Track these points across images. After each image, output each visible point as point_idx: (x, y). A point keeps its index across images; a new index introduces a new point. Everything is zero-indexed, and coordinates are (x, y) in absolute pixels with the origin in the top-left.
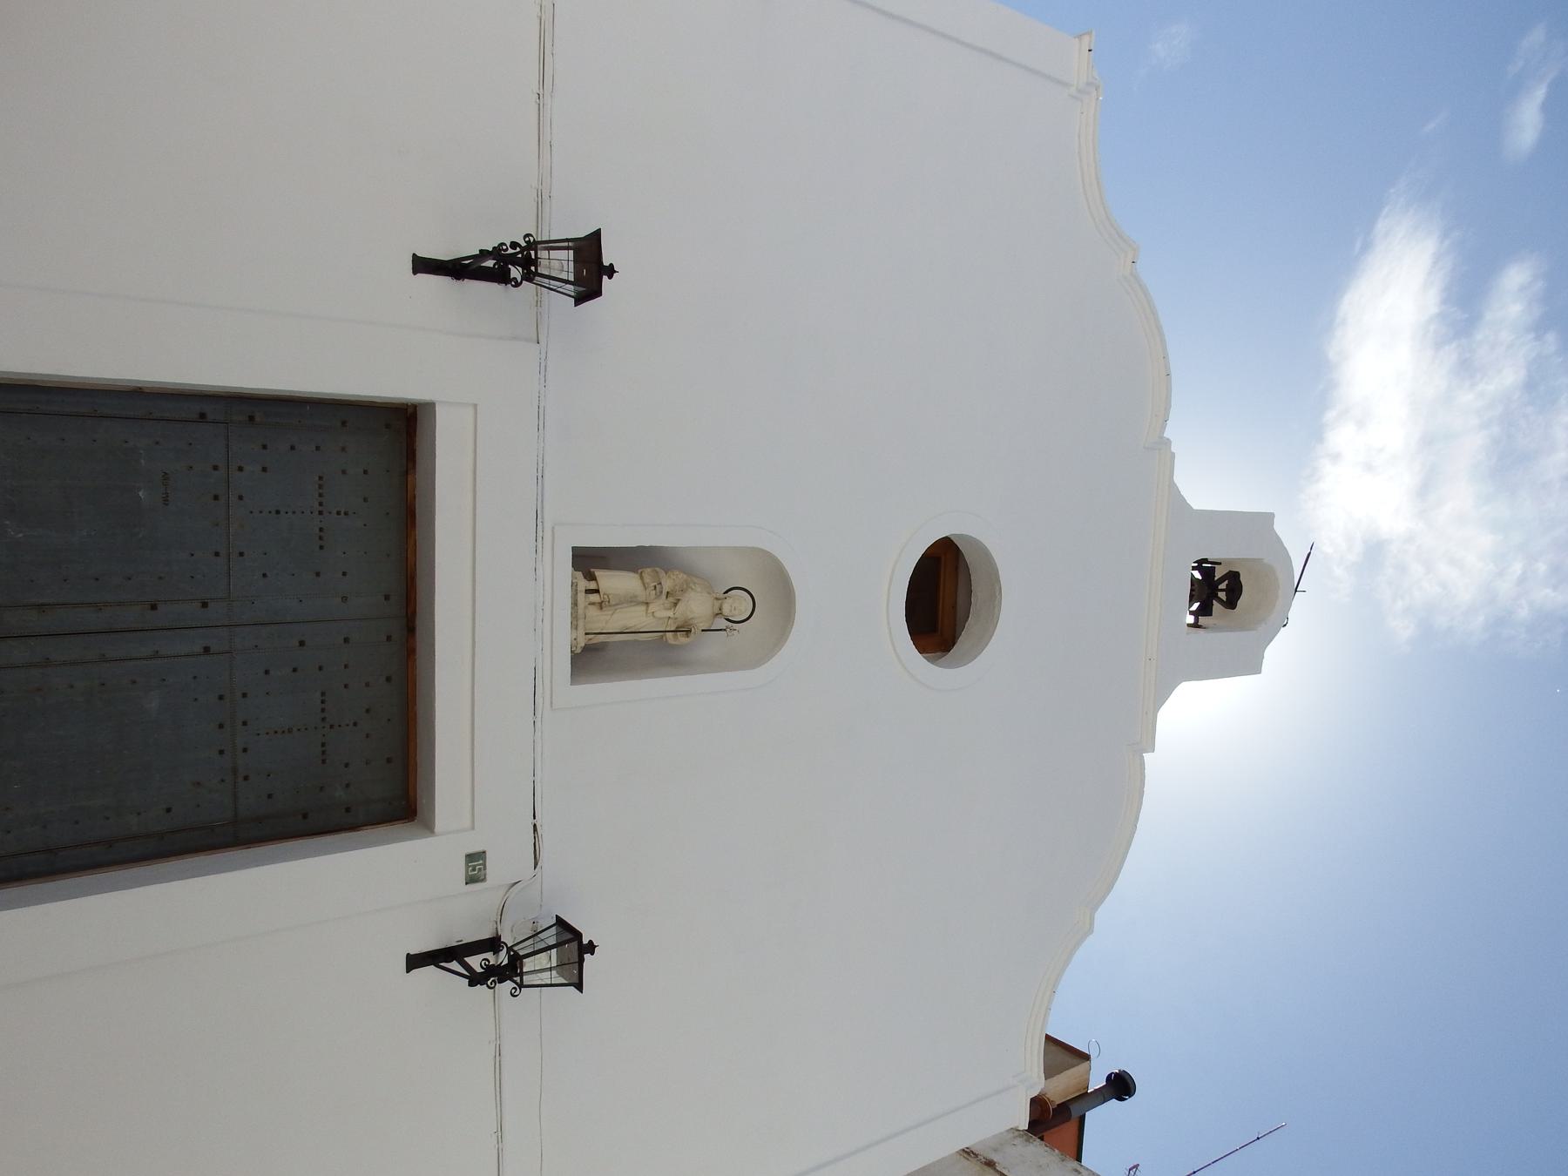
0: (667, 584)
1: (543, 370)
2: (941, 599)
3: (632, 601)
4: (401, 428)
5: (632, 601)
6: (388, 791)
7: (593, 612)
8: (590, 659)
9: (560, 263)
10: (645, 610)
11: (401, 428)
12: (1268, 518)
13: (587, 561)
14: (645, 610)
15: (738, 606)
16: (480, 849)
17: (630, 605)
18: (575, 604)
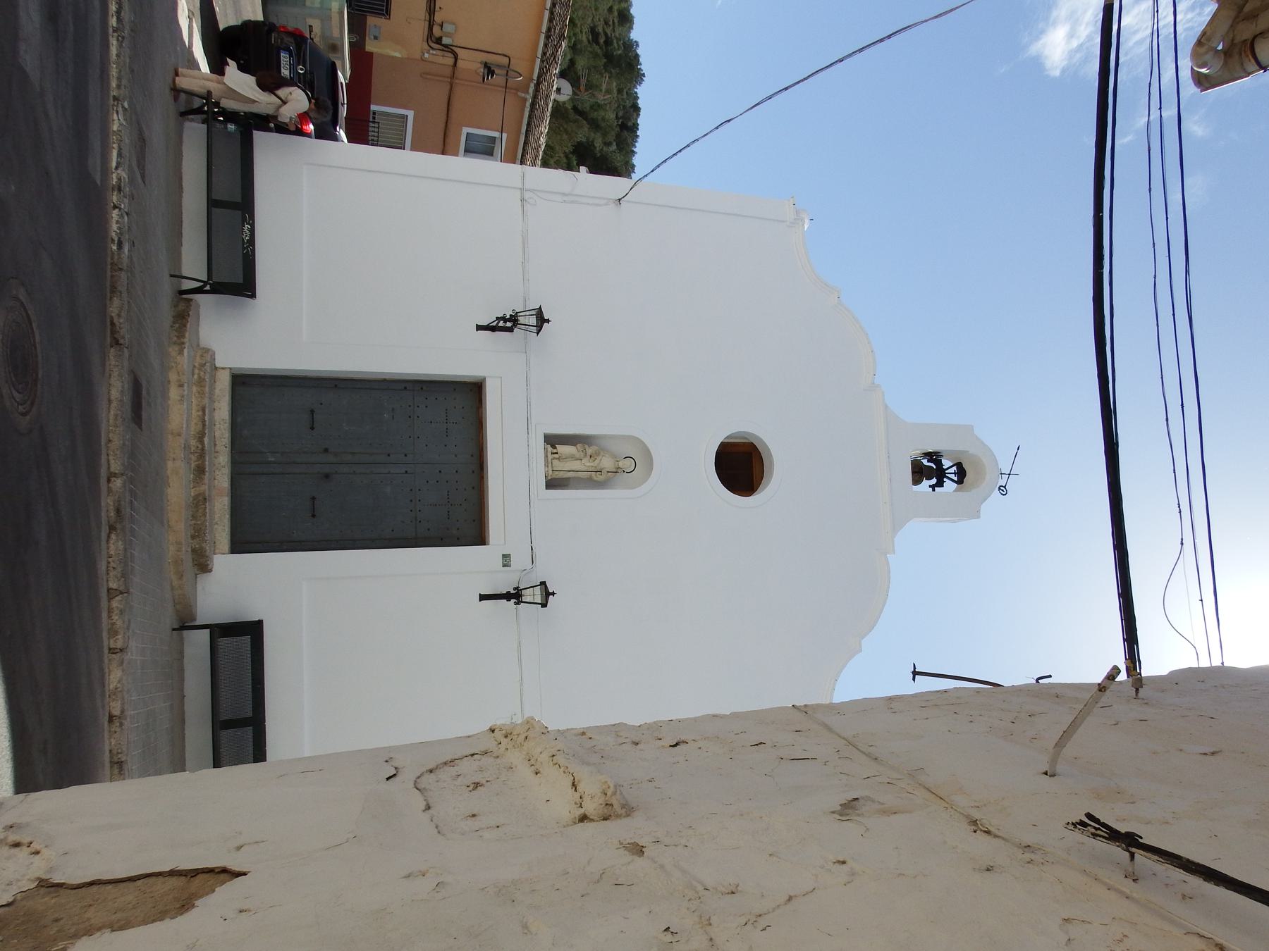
0: (589, 451)
1: (528, 363)
2: (740, 467)
3: (573, 458)
4: (476, 389)
5: (573, 458)
6: (473, 530)
7: (556, 462)
8: (552, 484)
9: (536, 595)
10: (578, 462)
11: (476, 389)
12: (971, 428)
13: (552, 441)
14: (578, 462)
15: (628, 465)
16: (664, 106)
17: (572, 461)
18: (546, 456)
